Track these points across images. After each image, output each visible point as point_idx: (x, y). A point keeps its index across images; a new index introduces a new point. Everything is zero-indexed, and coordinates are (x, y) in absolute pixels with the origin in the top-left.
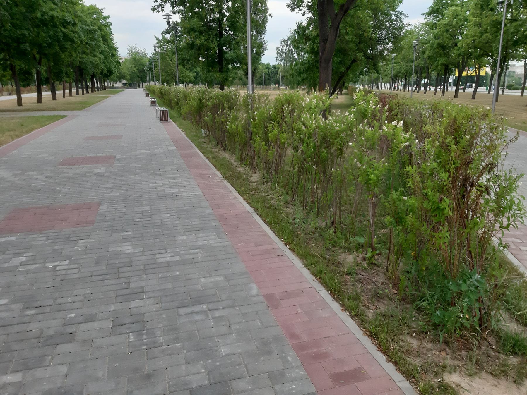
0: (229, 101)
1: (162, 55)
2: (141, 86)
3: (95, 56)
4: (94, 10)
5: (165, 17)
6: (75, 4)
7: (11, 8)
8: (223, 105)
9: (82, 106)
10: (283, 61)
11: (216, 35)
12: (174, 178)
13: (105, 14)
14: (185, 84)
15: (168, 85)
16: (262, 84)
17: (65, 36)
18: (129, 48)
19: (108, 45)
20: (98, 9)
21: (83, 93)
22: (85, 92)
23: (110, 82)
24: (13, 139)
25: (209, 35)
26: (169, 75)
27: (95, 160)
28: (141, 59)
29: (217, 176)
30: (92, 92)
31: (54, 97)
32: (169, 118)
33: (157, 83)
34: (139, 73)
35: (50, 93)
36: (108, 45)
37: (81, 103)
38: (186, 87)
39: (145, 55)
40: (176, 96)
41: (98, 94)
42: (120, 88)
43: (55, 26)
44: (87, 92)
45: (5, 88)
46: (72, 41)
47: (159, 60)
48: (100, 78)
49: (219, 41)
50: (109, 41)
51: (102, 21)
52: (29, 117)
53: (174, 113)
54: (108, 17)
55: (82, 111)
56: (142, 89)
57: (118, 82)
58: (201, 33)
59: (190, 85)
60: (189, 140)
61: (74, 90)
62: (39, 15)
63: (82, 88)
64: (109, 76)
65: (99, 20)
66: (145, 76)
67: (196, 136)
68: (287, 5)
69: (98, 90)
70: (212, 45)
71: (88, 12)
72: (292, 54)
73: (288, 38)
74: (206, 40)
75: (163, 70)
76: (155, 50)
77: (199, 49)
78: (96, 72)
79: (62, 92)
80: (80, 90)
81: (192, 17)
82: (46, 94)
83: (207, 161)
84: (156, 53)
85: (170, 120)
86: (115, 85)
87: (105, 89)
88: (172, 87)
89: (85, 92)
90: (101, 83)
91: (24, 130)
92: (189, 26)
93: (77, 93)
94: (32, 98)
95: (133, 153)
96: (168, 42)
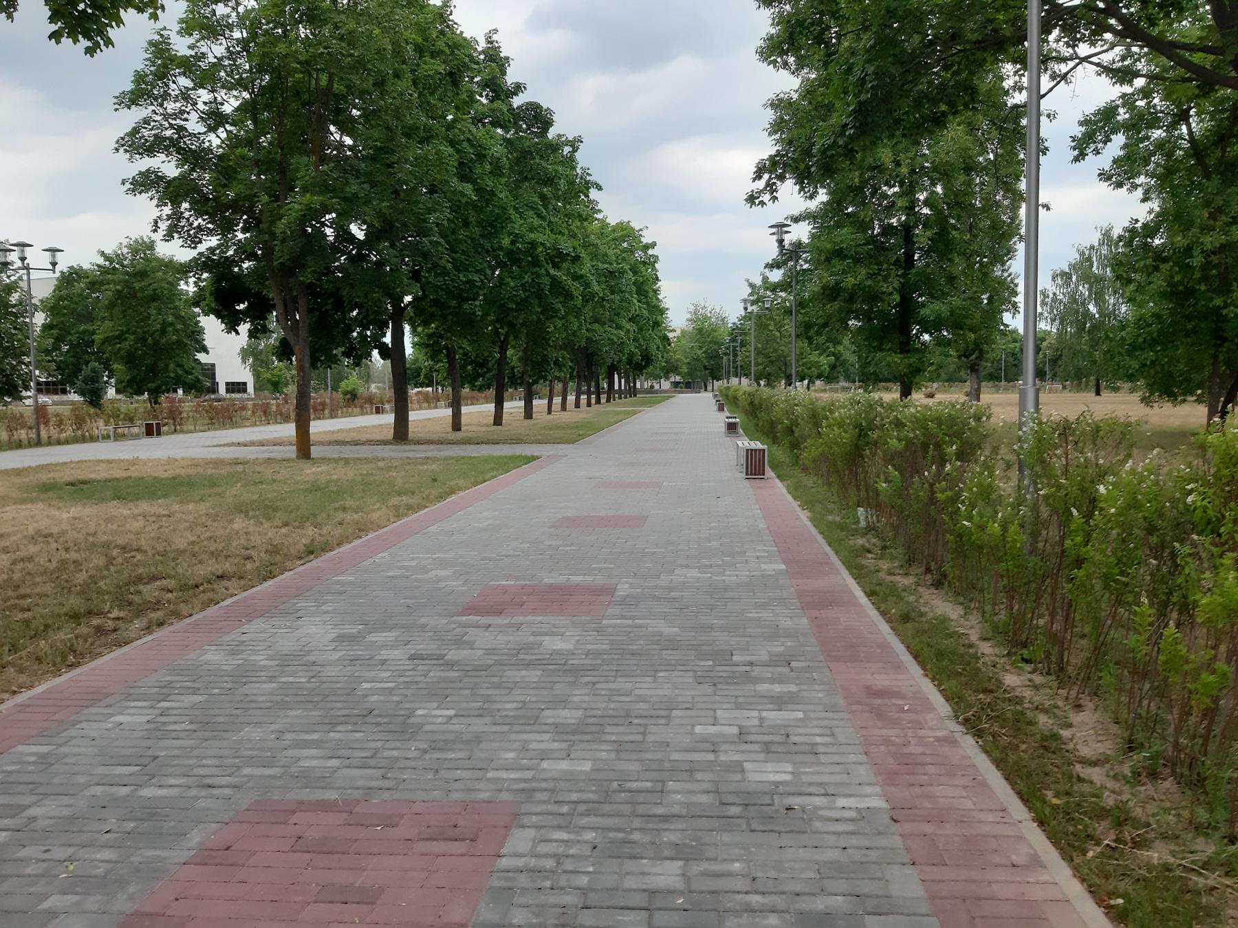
0: (958, 435)
1: (762, 317)
2: (710, 388)
3: (619, 327)
4: (625, 233)
5: (774, 230)
6: (586, 220)
7: (454, 231)
8: (938, 446)
9: (574, 435)
10: (1057, 322)
11: (897, 262)
12: (780, 702)
13: (645, 240)
14: (806, 382)
15: (769, 385)
16: (998, 379)
17: (555, 282)
18: (692, 309)
19: (647, 303)
20: (633, 229)
21: (589, 405)
22: (593, 401)
23: (646, 379)
24: (398, 517)
25: (880, 264)
26: (772, 362)
27: (557, 599)
29: (931, 709)
30: (608, 400)
31: (528, 413)
32: (767, 468)
33: (745, 381)
34: (710, 359)
36: (647, 303)
37: (577, 426)
38: (808, 388)
40: (789, 412)
41: (619, 406)
42: (665, 392)
43: (536, 263)
44: (598, 401)
46: (569, 296)
47: (752, 331)
48: (626, 372)
49: (903, 276)
50: (651, 294)
51: (639, 254)
52: (459, 459)
53: (781, 454)
54: (653, 245)
55: (574, 446)
56: (711, 394)
58: (858, 260)
59: (818, 382)
60: (820, 538)
61: (571, 398)
62: (506, 242)
63: (589, 393)
64: (645, 367)
65: (633, 252)
66: (719, 366)
67: (842, 527)
68: (1100, 175)
69: (620, 398)
70: (885, 287)
71: (612, 236)
72: (1083, 304)
73: (1073, 267)
74: (870, 276)
75: (759, 353)
76: (746, 309)
77: (851, 298)
78: (617, 359)
79: (546, 401)
80: (584, 397)
81: (839, 225)
82: (514, 407)
83: (885, 628)
84: (748, 317)
85: (769, 473)
86: (657, 387)
88: (776, 391)
89: (593, 401)
90: (627, 382)
91: (434, 493)
92: (829, 246)
93: (577, 405)
94: (440, 419)
95: (664, 580)
96: (774, 288)
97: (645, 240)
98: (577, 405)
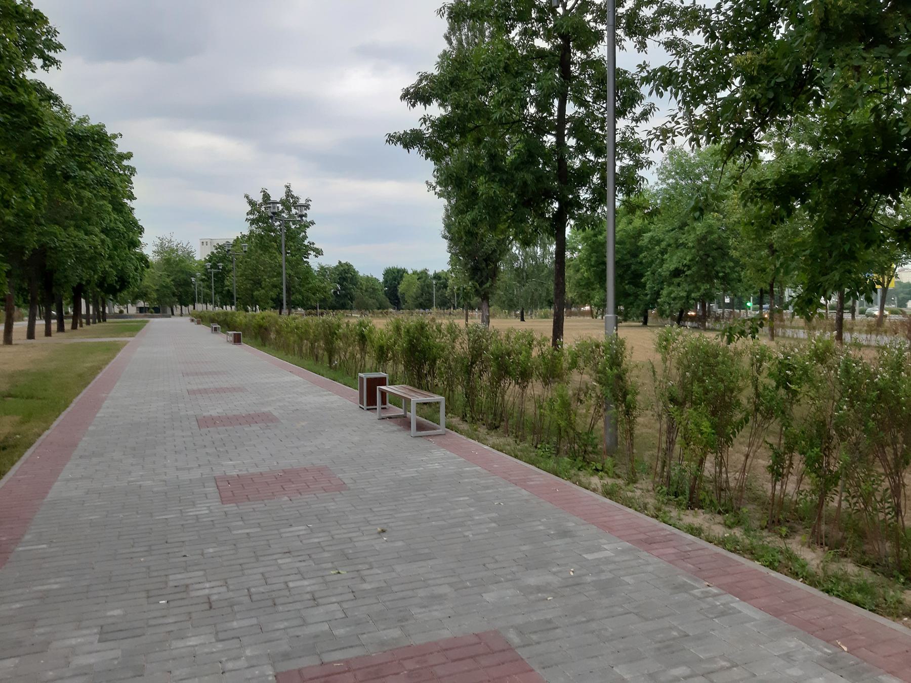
18: (158, 242)
21: (48, 333)
28: (182, 261)
30: (74, 327)
35: (44, 322)
39: (189, 255)
44: (61, 328)
45: (815, 300)
54: (129, 156)
57: (129, 305)
64: (120, 290)
69: (88, 323)
86: (125, 311)
87: (105, 320)
90: (96, 309)
97: (119, 150)
98: (31, 334)
